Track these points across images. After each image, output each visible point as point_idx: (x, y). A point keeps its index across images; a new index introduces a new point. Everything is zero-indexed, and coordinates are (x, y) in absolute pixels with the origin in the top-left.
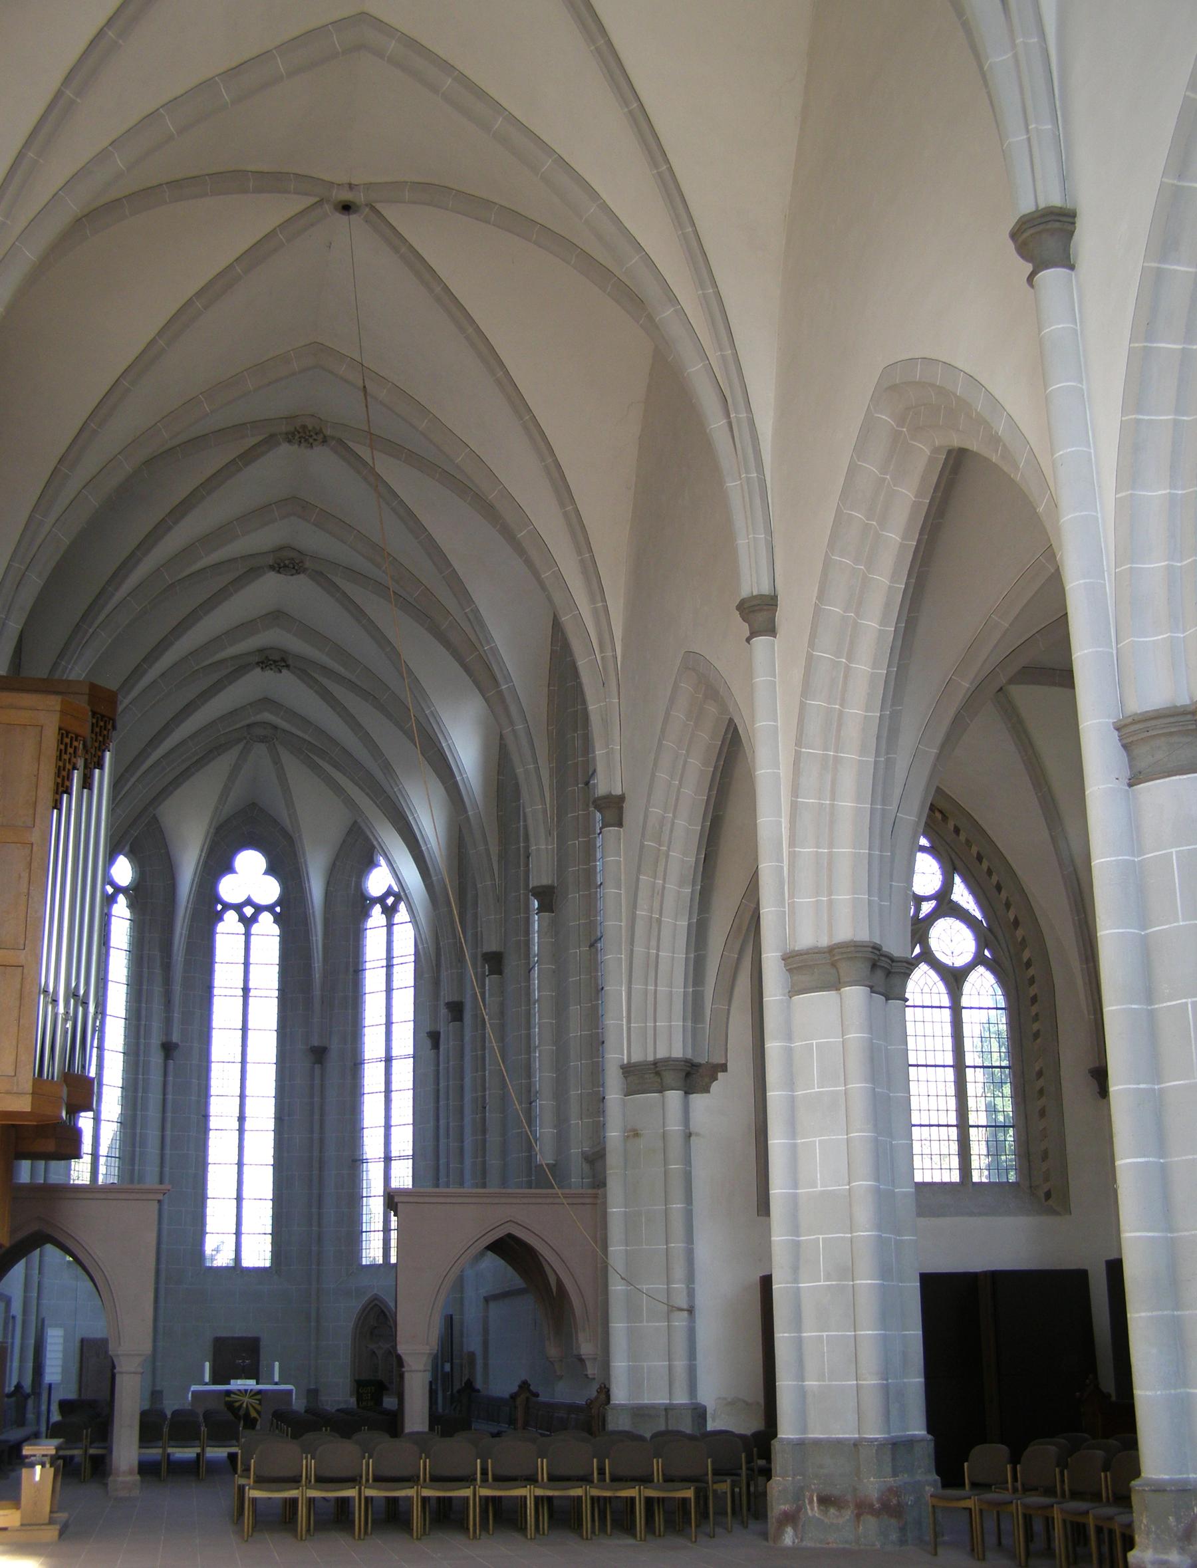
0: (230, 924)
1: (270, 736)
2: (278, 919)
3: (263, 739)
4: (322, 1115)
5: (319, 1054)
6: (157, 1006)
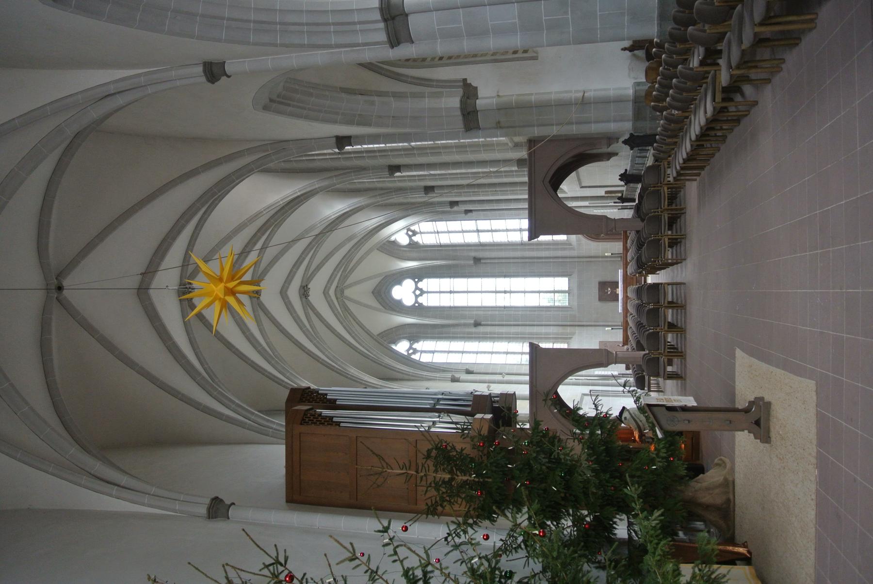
0: (424, 300)
1: (340, 291)
2: (420, 280)
3: (342, 292)
5: (477, 260)
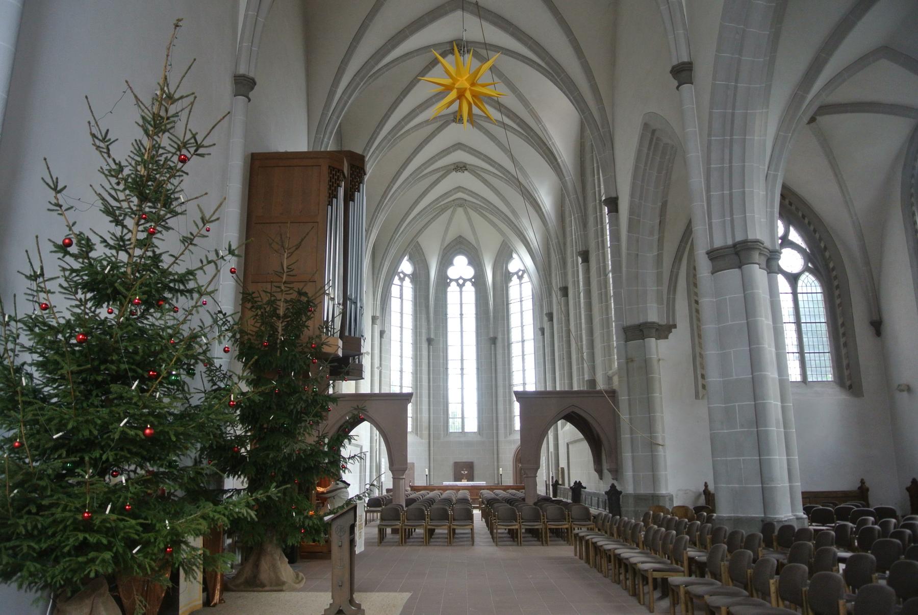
1: (462, 203)
2: (474, 284)
3: (460, 206)
4: (496, 366)
5: (494, 341)
6: (424, 323)
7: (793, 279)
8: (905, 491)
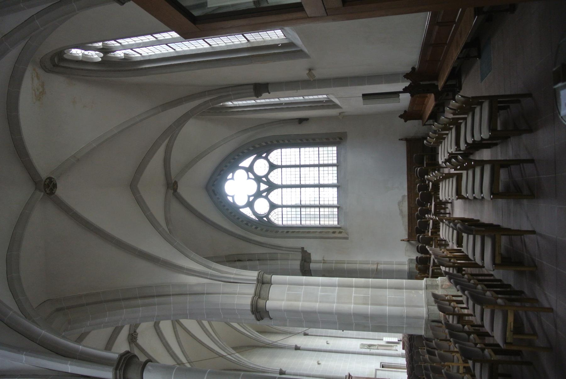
7: (273, 206)
8: (347, 374)
